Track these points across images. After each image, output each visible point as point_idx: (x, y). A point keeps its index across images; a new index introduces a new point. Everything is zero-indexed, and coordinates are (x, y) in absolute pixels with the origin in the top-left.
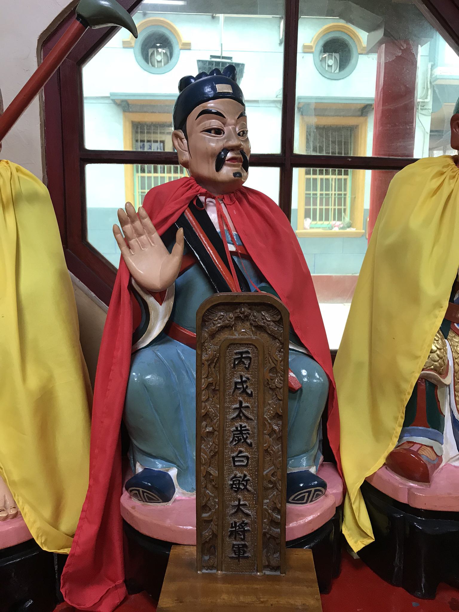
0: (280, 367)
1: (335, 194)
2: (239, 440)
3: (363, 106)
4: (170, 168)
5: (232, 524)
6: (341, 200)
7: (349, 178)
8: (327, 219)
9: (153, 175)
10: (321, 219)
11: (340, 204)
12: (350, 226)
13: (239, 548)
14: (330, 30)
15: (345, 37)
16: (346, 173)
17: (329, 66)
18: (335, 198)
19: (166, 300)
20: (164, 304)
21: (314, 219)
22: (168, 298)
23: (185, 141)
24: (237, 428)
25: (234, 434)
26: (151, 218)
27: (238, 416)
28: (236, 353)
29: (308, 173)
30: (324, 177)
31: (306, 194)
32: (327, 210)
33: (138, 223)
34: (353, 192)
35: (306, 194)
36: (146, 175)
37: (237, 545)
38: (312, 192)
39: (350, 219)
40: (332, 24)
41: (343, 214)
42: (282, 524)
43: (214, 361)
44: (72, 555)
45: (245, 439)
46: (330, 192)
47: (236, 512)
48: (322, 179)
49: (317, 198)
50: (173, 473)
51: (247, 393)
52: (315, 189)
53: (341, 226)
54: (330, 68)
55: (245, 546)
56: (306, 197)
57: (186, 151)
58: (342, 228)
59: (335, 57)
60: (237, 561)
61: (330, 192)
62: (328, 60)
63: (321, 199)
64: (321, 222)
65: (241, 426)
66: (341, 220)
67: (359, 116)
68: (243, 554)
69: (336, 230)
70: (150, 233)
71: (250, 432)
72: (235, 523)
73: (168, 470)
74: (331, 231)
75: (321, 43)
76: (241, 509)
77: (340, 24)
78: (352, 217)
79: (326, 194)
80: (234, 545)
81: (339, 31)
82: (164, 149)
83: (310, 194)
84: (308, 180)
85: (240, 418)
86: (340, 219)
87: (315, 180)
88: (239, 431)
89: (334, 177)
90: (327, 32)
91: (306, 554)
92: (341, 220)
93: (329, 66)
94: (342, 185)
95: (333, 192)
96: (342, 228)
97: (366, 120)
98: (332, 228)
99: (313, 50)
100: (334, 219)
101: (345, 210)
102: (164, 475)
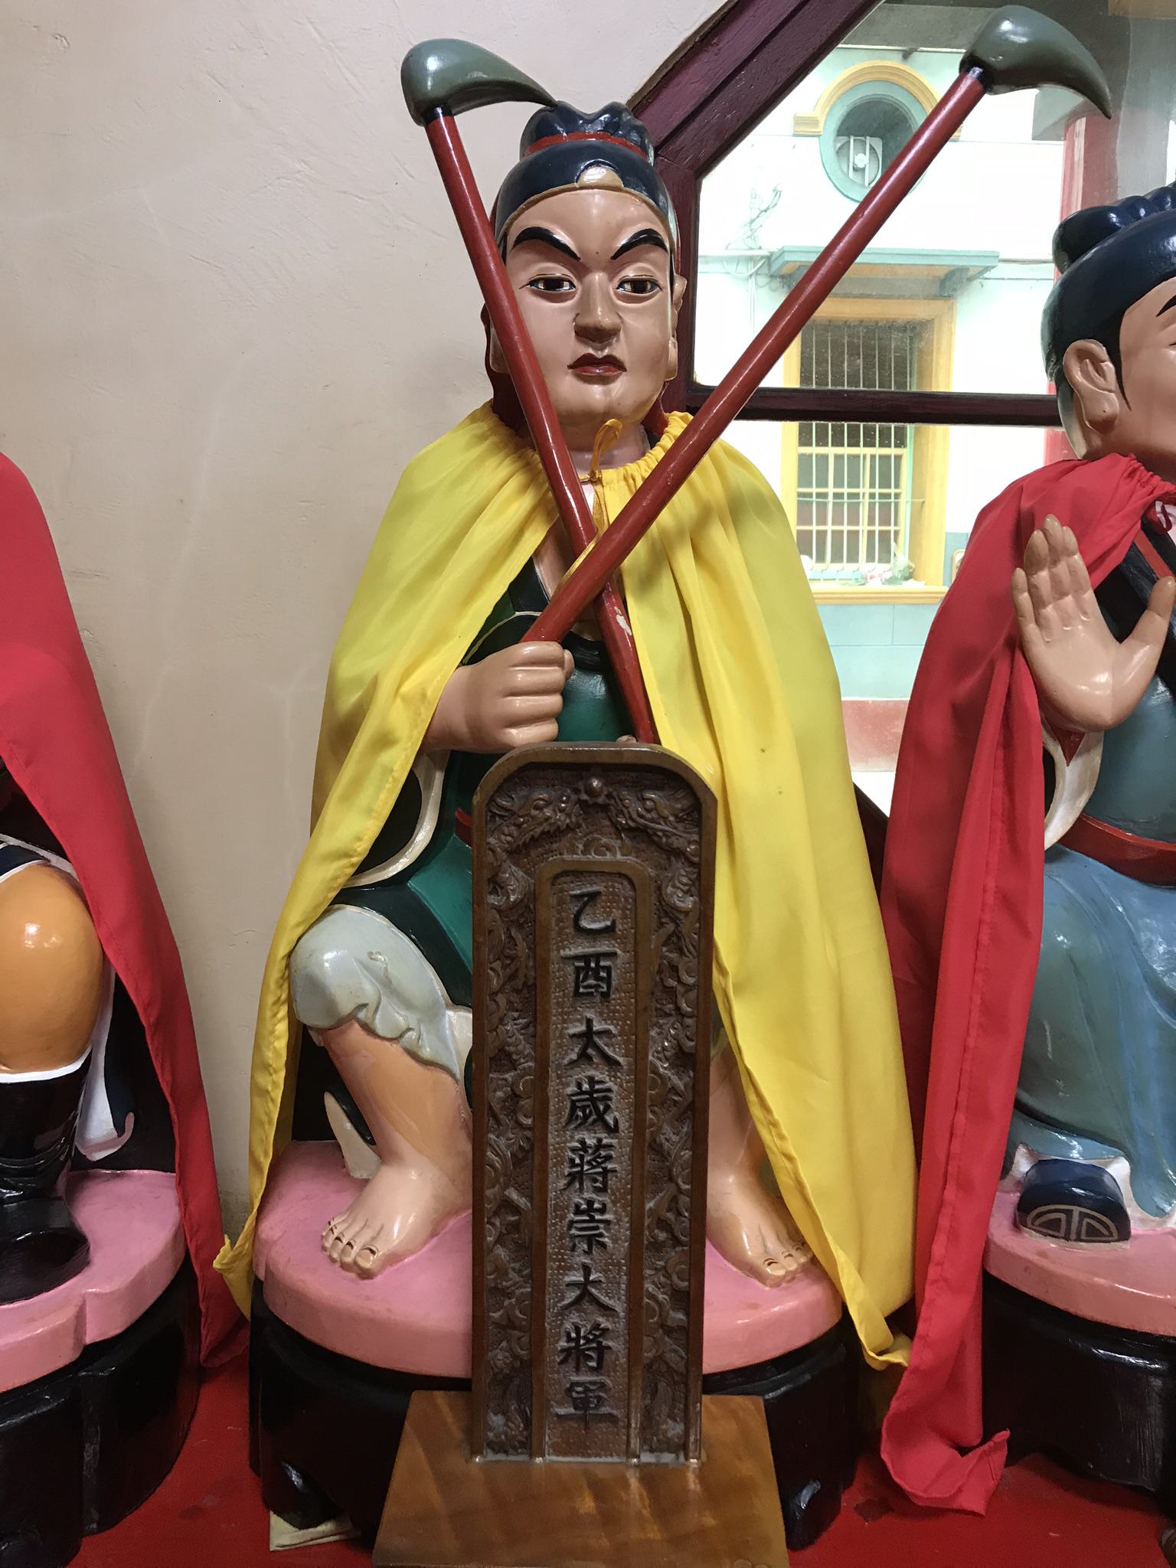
0: (688, 927)
1: (872, 496)
2: (586, 1117)
3: (942, 273)
4: (904, 429)
5: (568, 1334)
6: (886, 511)
7: (906, 453)
8: (853, 558)
9: (831, 451)
10: (837, 557)
11: (885, 521)
12: (910, 575)
13: (587, 1390)
14: (861, 79)
15: (900, 97)
16: (901, 442)
17: (855, 169)
18: (872, 506)
19: (1080, 754)
20: (1077, 764)
21: (821, 558)
22: (1088, 750)
23: (1109, 366)
24: (579, 1085)
25: (573, 1102)
26: (1084, 556)
27: (584, 1057)
28: (577, 958)
29: (804, 440)
30: (846, 450)
31: (800, 495)
32: (854, 535)
33: (1062, 568)
34: (918, 490)
35: (800, 495)
36: (814, 450)
37: (578, 1384)
38: (814, 490)
39: (911, 558)
40: (867, 64)
41: (893, 544)
42: (692, 1334)
43: (524, 914)
44: (916, 1370)
45: (601, 1118)
46: (860, 490)
47: (577, 1301)
48: (839, 458)
49: (825, 504)
50: (1119, 1170)
51: (606, 1124)
52: (822, 482)
53: (889, 575)
54: (859, 174)
55: (602, 1386)
56: (799, 502)
57: (1110, 391)
58: (891, 581)
59: (872, 148)
60: (597, 1027)
61: (860, 490)
62: (856, 153)
63: (838, 507)
64: (837, 566)
65: (592, 1081)
66: (889, 561)
67: (935, 298)
68: (597, 1407)
69: (875, 586)
70: (1078, 591)
71: (610, 1084)
72: (577, 1330)
73: (1108, 1164)
74: (862, 589)
75: (840, 112)
76: (591, 1294)
77: (888, 63)
78: (913, 554)
79: (851, 496)
80: (574, 1384)
81: (886, 81)
82: (869, 382)
83: (810, 495)
84: (804, 461)
85: (590, 1059)
86: (886, 556)
87: (823, 459)
88: (585, 1093)
89: (869, 451)
90: (855, 82)
91: (750, 1410)
92: (889, 561)
93: (855, 169)
94: (887, 473)
95: (868, 490)
96: (891, 581)
97: (951, 308)
98: (864, 580)
99: (820, 129)
100: (870, 558)
101: (896, 533)
102: (1093, 1178)
